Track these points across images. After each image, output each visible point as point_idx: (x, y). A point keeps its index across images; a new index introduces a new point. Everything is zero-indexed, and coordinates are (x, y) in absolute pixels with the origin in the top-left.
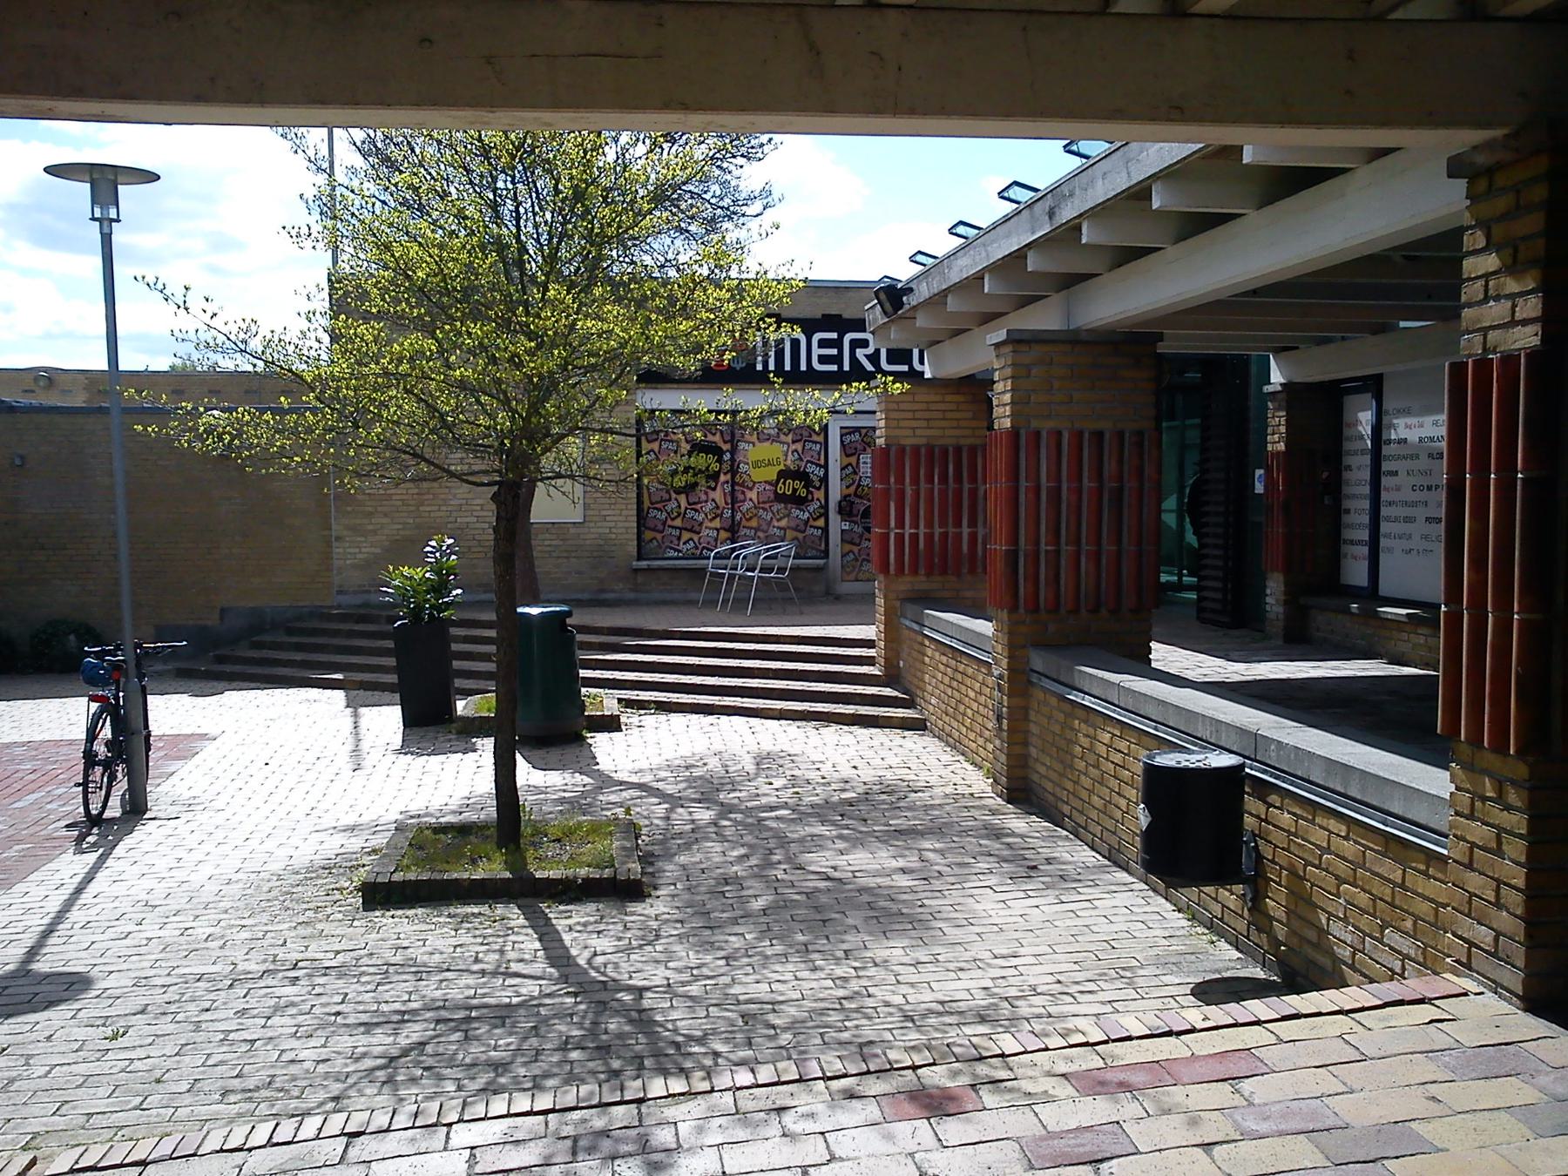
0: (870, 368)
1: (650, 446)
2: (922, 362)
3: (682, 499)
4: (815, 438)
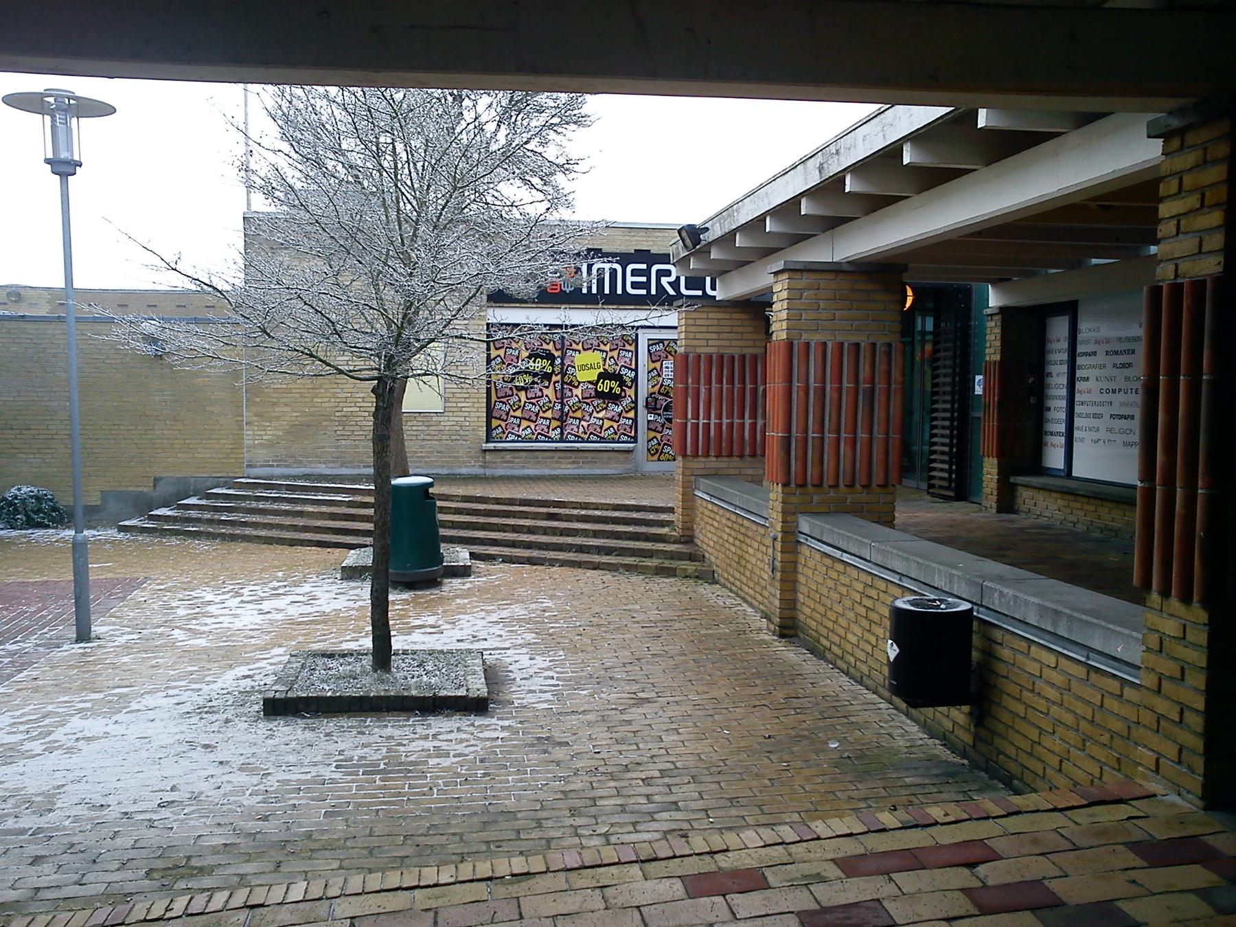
0: (672, 292)
1: (498, 352)
2: (713, 288)
3: (522, 395)
4: (628, 347)
